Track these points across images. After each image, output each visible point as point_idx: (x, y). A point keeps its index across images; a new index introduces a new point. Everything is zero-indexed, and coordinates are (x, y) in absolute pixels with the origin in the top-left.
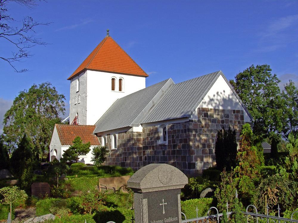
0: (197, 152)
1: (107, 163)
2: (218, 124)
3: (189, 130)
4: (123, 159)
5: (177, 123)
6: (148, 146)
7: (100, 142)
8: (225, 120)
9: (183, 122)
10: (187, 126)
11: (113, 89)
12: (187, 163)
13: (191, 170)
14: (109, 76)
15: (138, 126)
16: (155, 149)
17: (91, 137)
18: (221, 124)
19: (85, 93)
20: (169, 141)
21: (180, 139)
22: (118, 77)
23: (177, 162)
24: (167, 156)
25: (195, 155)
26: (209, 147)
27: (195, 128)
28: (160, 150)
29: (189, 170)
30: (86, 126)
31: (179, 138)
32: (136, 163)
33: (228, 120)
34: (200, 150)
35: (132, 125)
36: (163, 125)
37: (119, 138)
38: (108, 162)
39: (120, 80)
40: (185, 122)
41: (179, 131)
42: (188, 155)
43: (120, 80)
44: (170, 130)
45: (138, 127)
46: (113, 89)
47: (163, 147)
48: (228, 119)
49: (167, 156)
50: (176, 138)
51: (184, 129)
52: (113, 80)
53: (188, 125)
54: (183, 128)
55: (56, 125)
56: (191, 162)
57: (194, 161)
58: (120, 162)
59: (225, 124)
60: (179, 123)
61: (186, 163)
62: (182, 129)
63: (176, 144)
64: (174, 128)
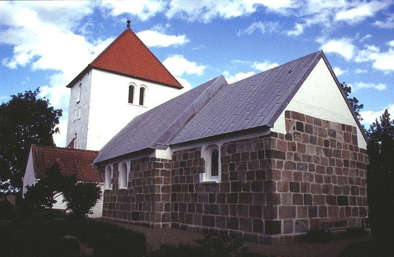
0: (285, 199)
1: (111, 211)
2: (319, 146)
3: (269, 153)
4: (137, 207)
5: (240, 141)
6: (296, 162)
7: (103, 178)
8: (331, 139)
9: (257, 138)
10: (266, 145)
11: (131, 100)
12: (263, 220)
13: (273, 236)
14: (127, 81)
15: (164, 148)
16: (195, 190)
17: (88, 168)
18: (324, 147)
19: (88, 102)
20: (224, 177)
21: (248, 171)
22: (138, 84)
23: (241, 219)
24: (218, 206)
25: (281, 205)
26: (305, 190)
27: (281, 149)
28: (204, 192)
29: (267, 236)
30: (85, 151)
31: (246, 170)
32: (159, 215)
33: (335, 140)
34: (291, 195)
35: (154, 146)
36: (213, 145)
37: (131, 170)
38: (112, 210)
39: (142, 90)
40: (260, 137)
41: (245, 156)
42: (266, 205)
43: (142, 90)
44: (227, 154)
45: (159, 33)
46: (131, 100)
47: (211, 187)
48: (334, 139)
49: (219, 204)
50: (238, 170)
51: (257, 151)
52: (131, 89)
53: (267, 141)
54: (255, 149)
55: (33, 145)
56: (274, 220)
57: (278, 217)
58: (131, 211)
59: (330, 147)
60: (248, 140)
61: (261, 220)
62: (253, 151)
63: (238, 181)
64: (235, 150)
